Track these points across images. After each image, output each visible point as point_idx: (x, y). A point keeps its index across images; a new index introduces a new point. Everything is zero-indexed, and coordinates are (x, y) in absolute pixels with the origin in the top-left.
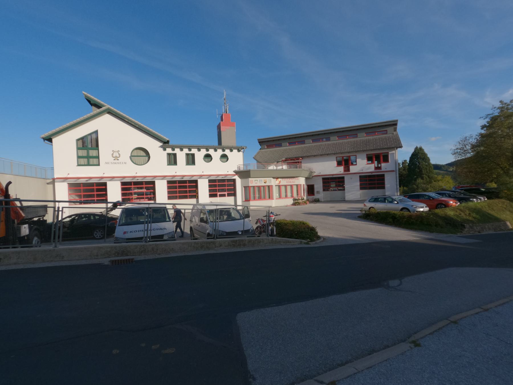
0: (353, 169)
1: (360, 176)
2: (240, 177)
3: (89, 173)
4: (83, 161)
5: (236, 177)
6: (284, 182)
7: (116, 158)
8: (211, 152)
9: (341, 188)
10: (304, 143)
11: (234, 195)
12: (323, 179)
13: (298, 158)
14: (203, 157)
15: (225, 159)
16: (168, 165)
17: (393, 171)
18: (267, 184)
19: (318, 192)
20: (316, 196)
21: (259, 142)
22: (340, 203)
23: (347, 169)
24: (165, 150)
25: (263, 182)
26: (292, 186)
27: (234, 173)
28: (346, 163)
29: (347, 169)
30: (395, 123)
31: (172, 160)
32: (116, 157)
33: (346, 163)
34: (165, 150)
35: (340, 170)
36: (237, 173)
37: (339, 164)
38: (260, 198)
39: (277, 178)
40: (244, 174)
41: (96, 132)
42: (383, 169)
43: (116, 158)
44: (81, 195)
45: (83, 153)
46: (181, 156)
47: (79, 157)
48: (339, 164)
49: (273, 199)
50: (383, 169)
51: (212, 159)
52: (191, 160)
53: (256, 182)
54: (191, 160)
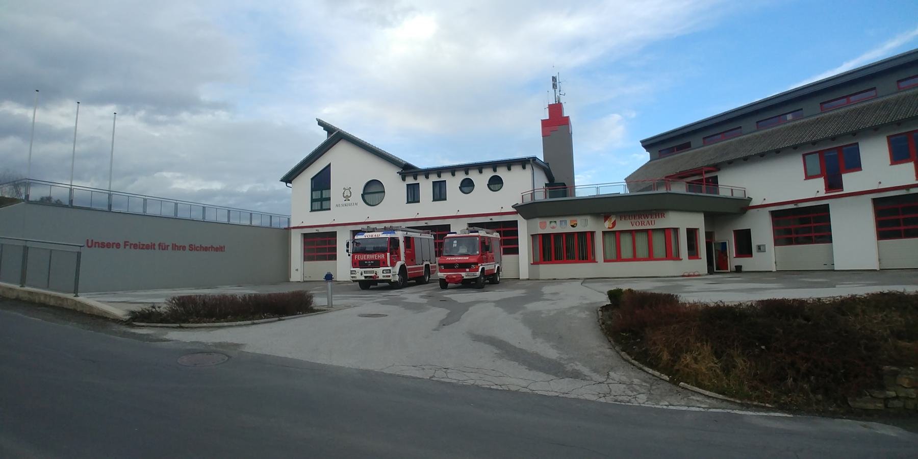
0: (851, 181)
2: (527, 217)
3: (321, 219)
4: (317, 205)
6: (624, 225)
7: (347, 198)
15: (497, 186)
16: (408, 202)
17: (229, 220)
18: (579, 229)
23: (833, 184)
24: (404, 179)
25: (569, 224)
28: (835, 164)
29: (833, 184)
31: (413, 195)
32: (347, 197)
34: (404, 179)
35: (816, 188)
36: (521, 209)
38: (650, 257)
39: (606, 217)
40: (528, 210)
43: (347, 198)
44: (791, 238)
45: (317, 195)
46: (426, 187)
47: (313, 201)
52: (440, 193)
53: (553, 224)
54: (440, 193)
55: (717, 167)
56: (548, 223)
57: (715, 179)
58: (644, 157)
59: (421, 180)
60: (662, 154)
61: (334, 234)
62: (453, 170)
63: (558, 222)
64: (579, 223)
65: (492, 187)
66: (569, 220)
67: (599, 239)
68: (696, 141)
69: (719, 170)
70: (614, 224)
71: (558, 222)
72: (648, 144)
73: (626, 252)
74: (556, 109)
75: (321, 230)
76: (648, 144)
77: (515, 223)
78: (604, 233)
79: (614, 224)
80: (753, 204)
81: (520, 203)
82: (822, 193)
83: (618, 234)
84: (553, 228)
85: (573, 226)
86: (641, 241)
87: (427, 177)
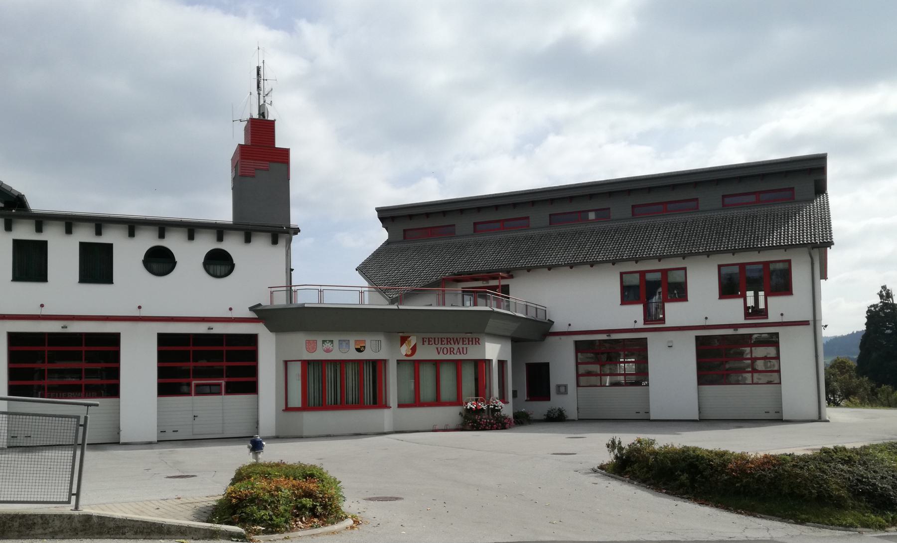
1: (698, 338)
2: (272, 329)
5: (259, 329)
8: (174, 243)
9: (296, 400)
10: (527, 227)
11: (251, 388)
12: (701, 342)
13: (492, 275)
14: (202, 259)
15: (219, 269)
17: (805, 323)
18: (367, 355)
19: (562, 389)
20: (556, 401)
21: (382, 219)
22: (639, 423)
23: (653, 318)
25: (353, 346)
26: (458, 364)
27: (252, 315)
28: (652, 292)
29: (653, 318)
30: (814, 165)
33: (652, 292)
34: (8, 228)
37: (629, 295)
41: (884, 287)
42: (773, 317)
48: (629, 295)
49: (386, 406)
50: (773, 317)
51: (232, 266)
52: (96, 266)
53: (328, 345)
54: (96, 266)
55: (510, 274)
56: (320, 343)
57: (506, 290)
58: (382, 235)
59: (53, 237)
60: (407, 235)
61: (114, 340)
62: (132, 226)
63: (336, 343)
64: (368, 345)
65: (211, 268)
66: (353, 339)
67: (392, 372)
68: (464, 225)
69: (511, 277)
70: (414, 349)
71: (336, 343)
72: (388, 216)
73: (427, 392)
74: (261, 129)
75: (220, 329)
76: (388, 216)
77: (253, 339)
78: (399, 362)
79: (414, 349)
80: (557, 328)
81: (265, 302)
82: (640, 324)
83: (417, 364)
84: (328, 351)
85: (359, 350)
86: (447, 376)
87: (69, 231)
